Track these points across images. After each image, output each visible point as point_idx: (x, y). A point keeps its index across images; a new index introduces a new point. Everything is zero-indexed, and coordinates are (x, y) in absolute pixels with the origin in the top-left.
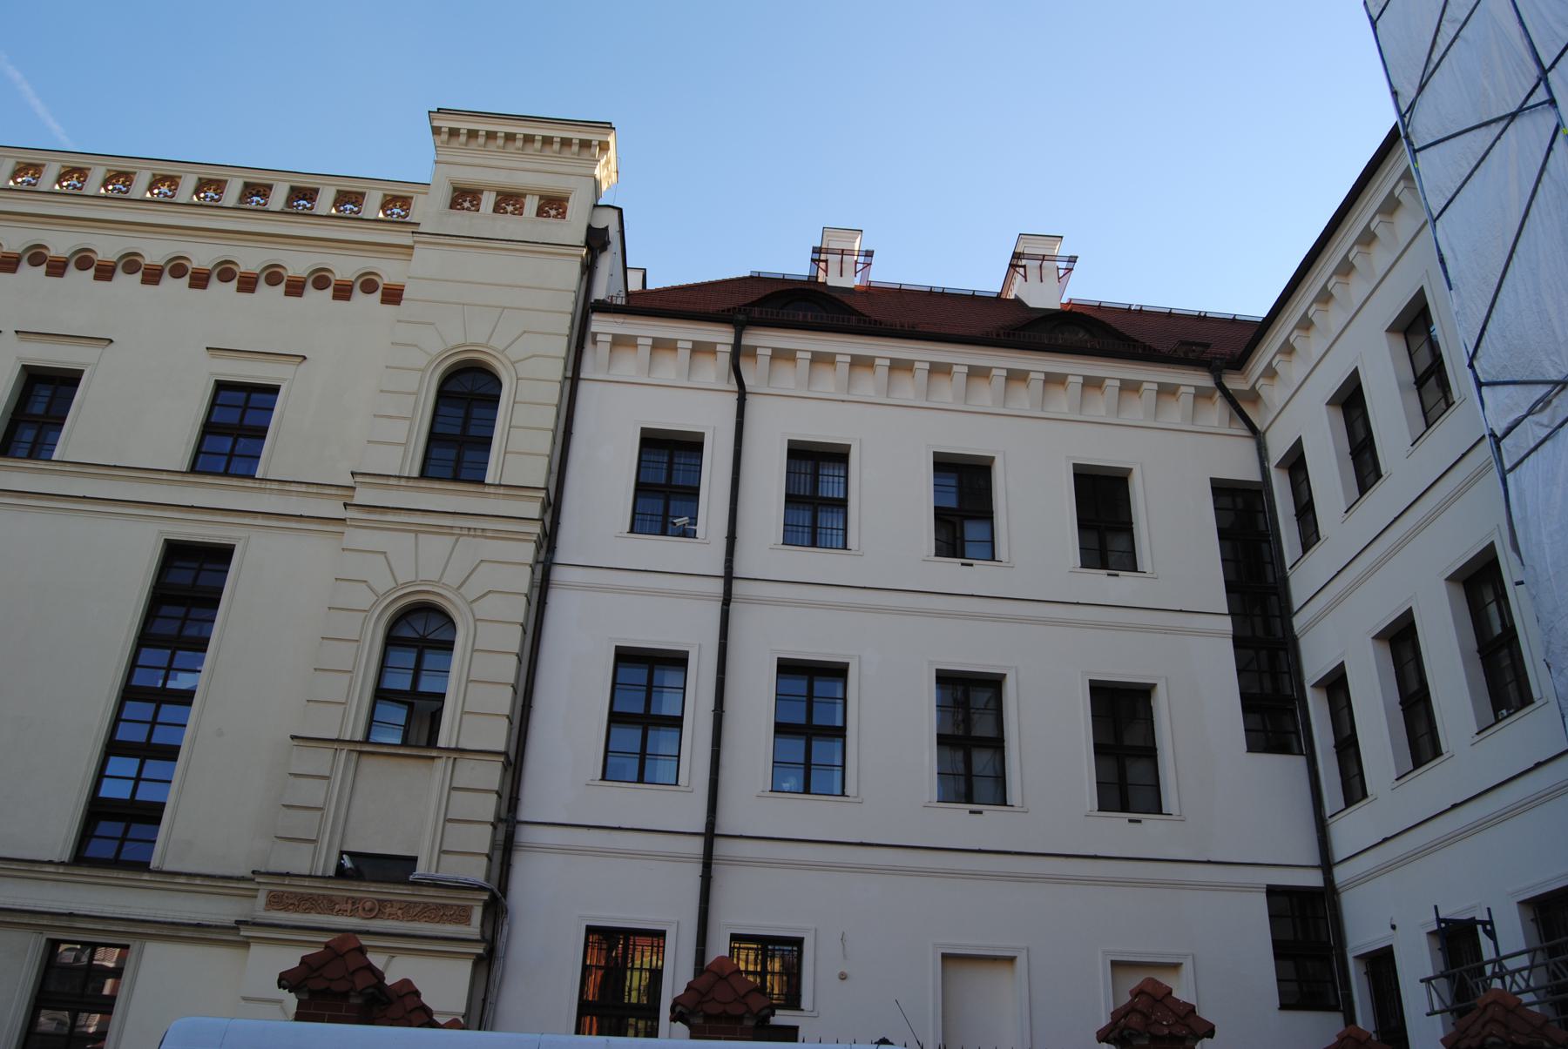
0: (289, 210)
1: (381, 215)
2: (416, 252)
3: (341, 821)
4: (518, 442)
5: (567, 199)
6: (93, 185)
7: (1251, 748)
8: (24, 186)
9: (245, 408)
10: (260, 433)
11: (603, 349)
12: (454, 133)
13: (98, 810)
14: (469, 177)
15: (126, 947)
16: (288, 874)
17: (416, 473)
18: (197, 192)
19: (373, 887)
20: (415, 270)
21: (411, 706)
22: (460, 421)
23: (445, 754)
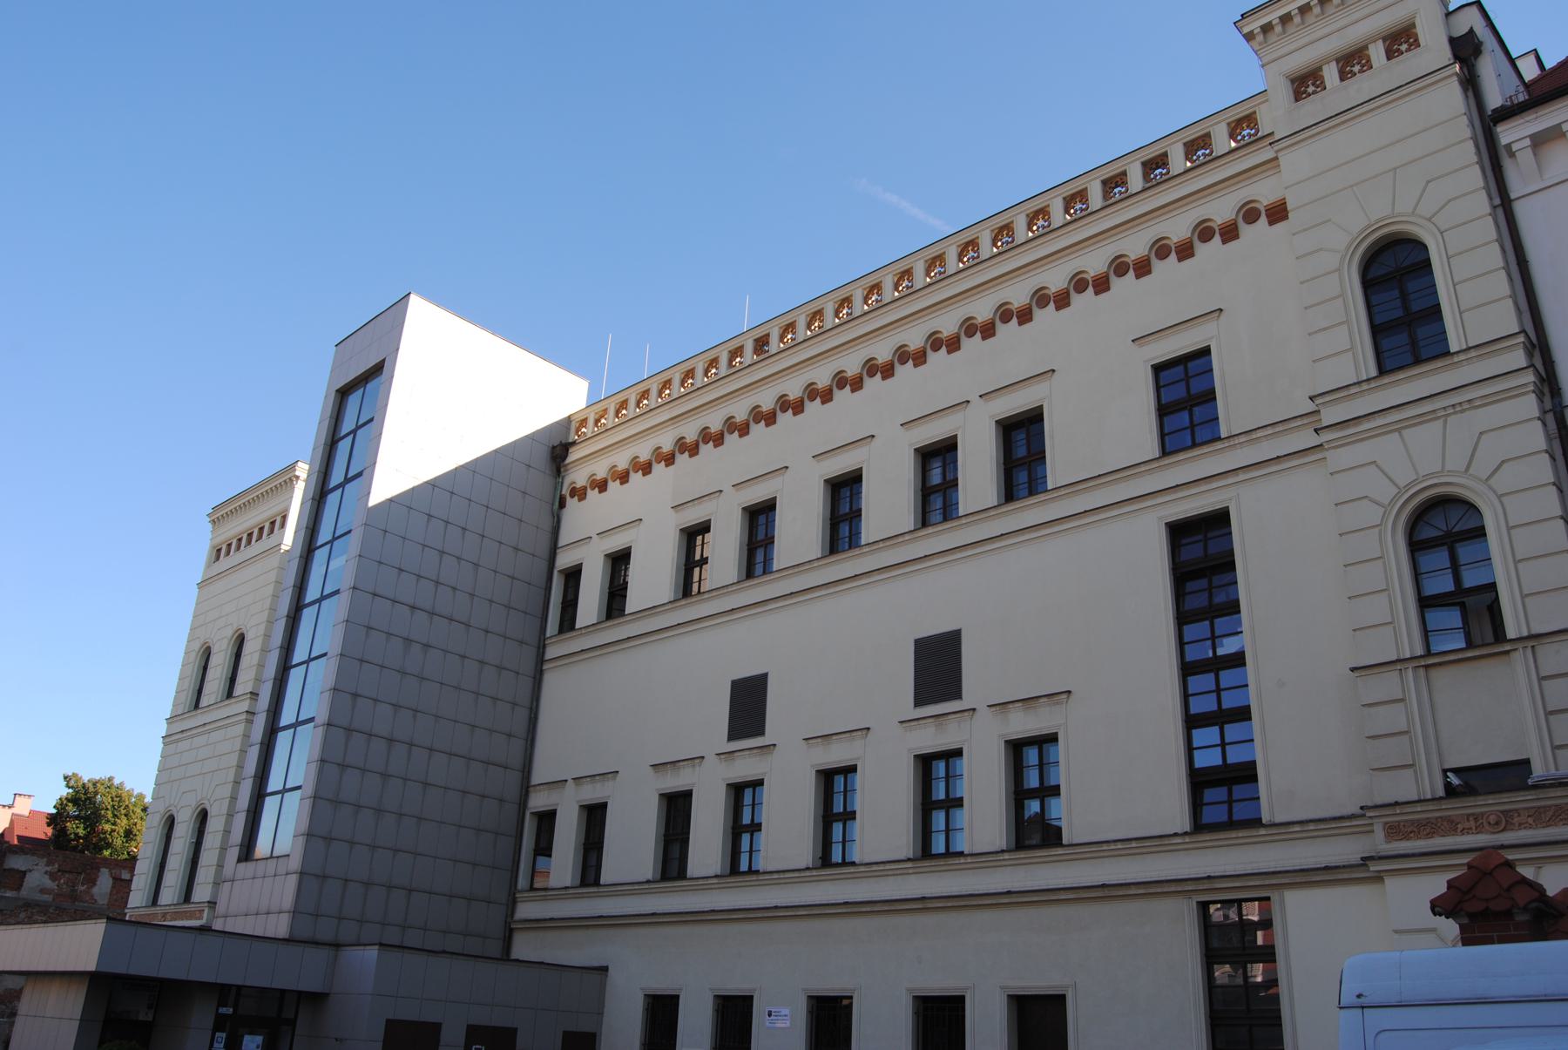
0: (1150, 184)
1: (1233, 144)
2: (1282, 161)
3: (1433, 740)
4: (1471, 296)
5: (1413, 25)
6: (1058, 216)
7: (917, 642)
8: (972, 262)
9: (1187, 379)
10: (1209, 396)
11: (1525, 157)
12: (1267, 29)
13: (1199, 781)
14: (1300, 61)
15: (1268, 899)
16: (1397, 804)
17: (1373, 372)
18: (1067, 211)
19: (1491, 799)
20: (1294, 175)
21: (1462, 606)
22: (1398, 303)
23: (1520, 645)
